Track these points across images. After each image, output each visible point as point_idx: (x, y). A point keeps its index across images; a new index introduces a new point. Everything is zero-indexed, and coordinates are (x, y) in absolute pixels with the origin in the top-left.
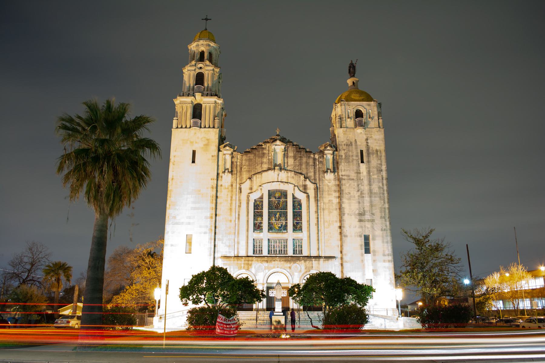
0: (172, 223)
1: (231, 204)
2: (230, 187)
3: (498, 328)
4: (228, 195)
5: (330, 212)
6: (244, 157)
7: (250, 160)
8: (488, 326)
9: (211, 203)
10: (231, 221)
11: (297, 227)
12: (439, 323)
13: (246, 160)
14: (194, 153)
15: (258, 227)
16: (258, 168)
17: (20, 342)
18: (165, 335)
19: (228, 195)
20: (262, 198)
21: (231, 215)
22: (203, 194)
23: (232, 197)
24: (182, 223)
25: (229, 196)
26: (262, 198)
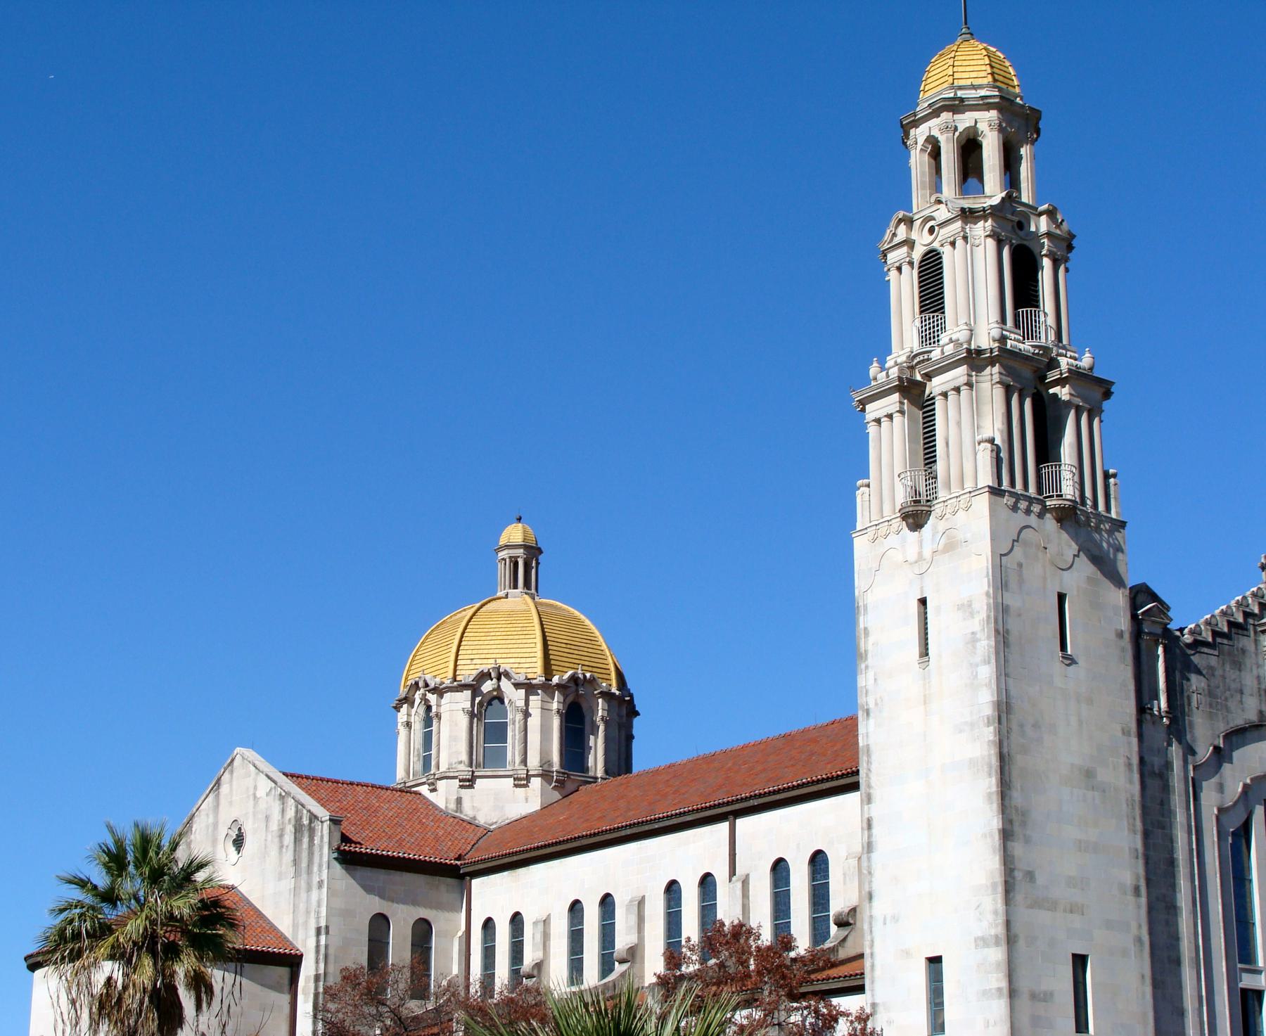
9: (1129, 829)
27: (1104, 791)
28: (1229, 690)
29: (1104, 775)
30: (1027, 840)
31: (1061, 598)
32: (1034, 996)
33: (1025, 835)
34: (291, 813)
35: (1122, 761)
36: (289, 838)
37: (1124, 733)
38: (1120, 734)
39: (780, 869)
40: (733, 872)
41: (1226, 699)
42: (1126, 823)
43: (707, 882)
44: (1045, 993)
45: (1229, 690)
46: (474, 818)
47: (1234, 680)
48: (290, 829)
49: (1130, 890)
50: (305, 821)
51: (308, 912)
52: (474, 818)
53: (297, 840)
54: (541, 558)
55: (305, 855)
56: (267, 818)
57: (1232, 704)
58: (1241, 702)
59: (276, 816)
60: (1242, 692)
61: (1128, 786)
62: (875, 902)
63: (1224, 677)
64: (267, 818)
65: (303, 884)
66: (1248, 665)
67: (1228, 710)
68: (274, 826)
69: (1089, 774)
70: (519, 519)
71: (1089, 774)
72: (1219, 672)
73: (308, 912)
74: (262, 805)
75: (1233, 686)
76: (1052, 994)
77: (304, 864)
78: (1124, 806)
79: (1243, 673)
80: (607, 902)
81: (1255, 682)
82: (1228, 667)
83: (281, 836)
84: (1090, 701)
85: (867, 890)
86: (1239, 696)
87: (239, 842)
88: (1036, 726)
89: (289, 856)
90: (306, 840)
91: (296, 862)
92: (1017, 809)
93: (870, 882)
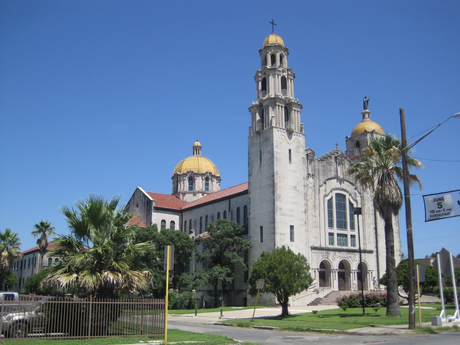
0: (279, 214)
1: (315, 201)
2: (313, 188)
3: (358, 325)
4: (312, 194)
5: (369, 217)
6: (320, 164)
7: (324, 166)
8: (382, 331)
9: (304, 199)
10: (315, 216)
11: (352, 227)
12: (362, 163)
13: (322, 166)
14: (290, 151)
15: (331, 225)
16: (329, 174)
17: (381, 333)
18: (33, 336)
19: (312, 194)
20: (332, 198)
21: (315, 212)
22: (298, 191)
23: (315, 196)
24: (286, 215)
25: (313, 195)
26: (332, 198)
27: (298, 191)
28: (328, 170)
29: (298, 188)
30: (280, 201)
31: (290, 151)
32: (281, 234)
33: (280, 200)
34: (146, 200)
35: (303, 185)
36: (146, 205)
37: (303, 179)
38: (302, 179)
39: (238, 209)
40: (229, 210)
41: (327, 172)
42: (303, 198)
43: (225, 212)
44: (283, 233)
45: (328, 170)
46: (186, 201)
47: (329, 168)
48: (146, 203)
49: (304, 212)
50: (149, 201)
51: (149, 220)
52: (186, 201)
53: (147, 205)
54: (202, 149)
55: (148, 208)
56: (142, 201)
57: (329, 173)
58: (331, 173)
59: (144, 200)
60: (331, 171)
61: (304, 190)
62: (251, 215)
63: (327, 168)
64: (142, 201)
65: (148, 214)
66: (332, 165)
67: (328, 174)
68: (143, 202)
69: (295, 187)
70: (197, 141)
71: (295, 187)
72: (326, 167)
73: (149, 220)
74: (141, 198)
75: (329, 169)
76: (285, 234)
77: (148, 210)
78: (303, 194)
79: (331, 167)
80: (207, 217)
81: (334, 169)
82: (328, 165)
83: (145, 204)
84: (296, 172)
85: (249, 212)
86: (330, 171)
87: (137, 206)
88: (283, 177)
89: (146, 208)
90: (149, 205)
91: (147, 209)
92: (278, 195)
93: (250, 211)
